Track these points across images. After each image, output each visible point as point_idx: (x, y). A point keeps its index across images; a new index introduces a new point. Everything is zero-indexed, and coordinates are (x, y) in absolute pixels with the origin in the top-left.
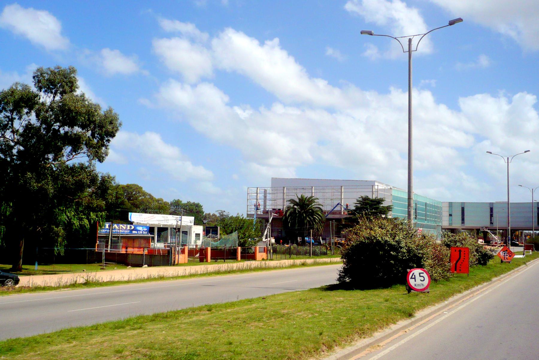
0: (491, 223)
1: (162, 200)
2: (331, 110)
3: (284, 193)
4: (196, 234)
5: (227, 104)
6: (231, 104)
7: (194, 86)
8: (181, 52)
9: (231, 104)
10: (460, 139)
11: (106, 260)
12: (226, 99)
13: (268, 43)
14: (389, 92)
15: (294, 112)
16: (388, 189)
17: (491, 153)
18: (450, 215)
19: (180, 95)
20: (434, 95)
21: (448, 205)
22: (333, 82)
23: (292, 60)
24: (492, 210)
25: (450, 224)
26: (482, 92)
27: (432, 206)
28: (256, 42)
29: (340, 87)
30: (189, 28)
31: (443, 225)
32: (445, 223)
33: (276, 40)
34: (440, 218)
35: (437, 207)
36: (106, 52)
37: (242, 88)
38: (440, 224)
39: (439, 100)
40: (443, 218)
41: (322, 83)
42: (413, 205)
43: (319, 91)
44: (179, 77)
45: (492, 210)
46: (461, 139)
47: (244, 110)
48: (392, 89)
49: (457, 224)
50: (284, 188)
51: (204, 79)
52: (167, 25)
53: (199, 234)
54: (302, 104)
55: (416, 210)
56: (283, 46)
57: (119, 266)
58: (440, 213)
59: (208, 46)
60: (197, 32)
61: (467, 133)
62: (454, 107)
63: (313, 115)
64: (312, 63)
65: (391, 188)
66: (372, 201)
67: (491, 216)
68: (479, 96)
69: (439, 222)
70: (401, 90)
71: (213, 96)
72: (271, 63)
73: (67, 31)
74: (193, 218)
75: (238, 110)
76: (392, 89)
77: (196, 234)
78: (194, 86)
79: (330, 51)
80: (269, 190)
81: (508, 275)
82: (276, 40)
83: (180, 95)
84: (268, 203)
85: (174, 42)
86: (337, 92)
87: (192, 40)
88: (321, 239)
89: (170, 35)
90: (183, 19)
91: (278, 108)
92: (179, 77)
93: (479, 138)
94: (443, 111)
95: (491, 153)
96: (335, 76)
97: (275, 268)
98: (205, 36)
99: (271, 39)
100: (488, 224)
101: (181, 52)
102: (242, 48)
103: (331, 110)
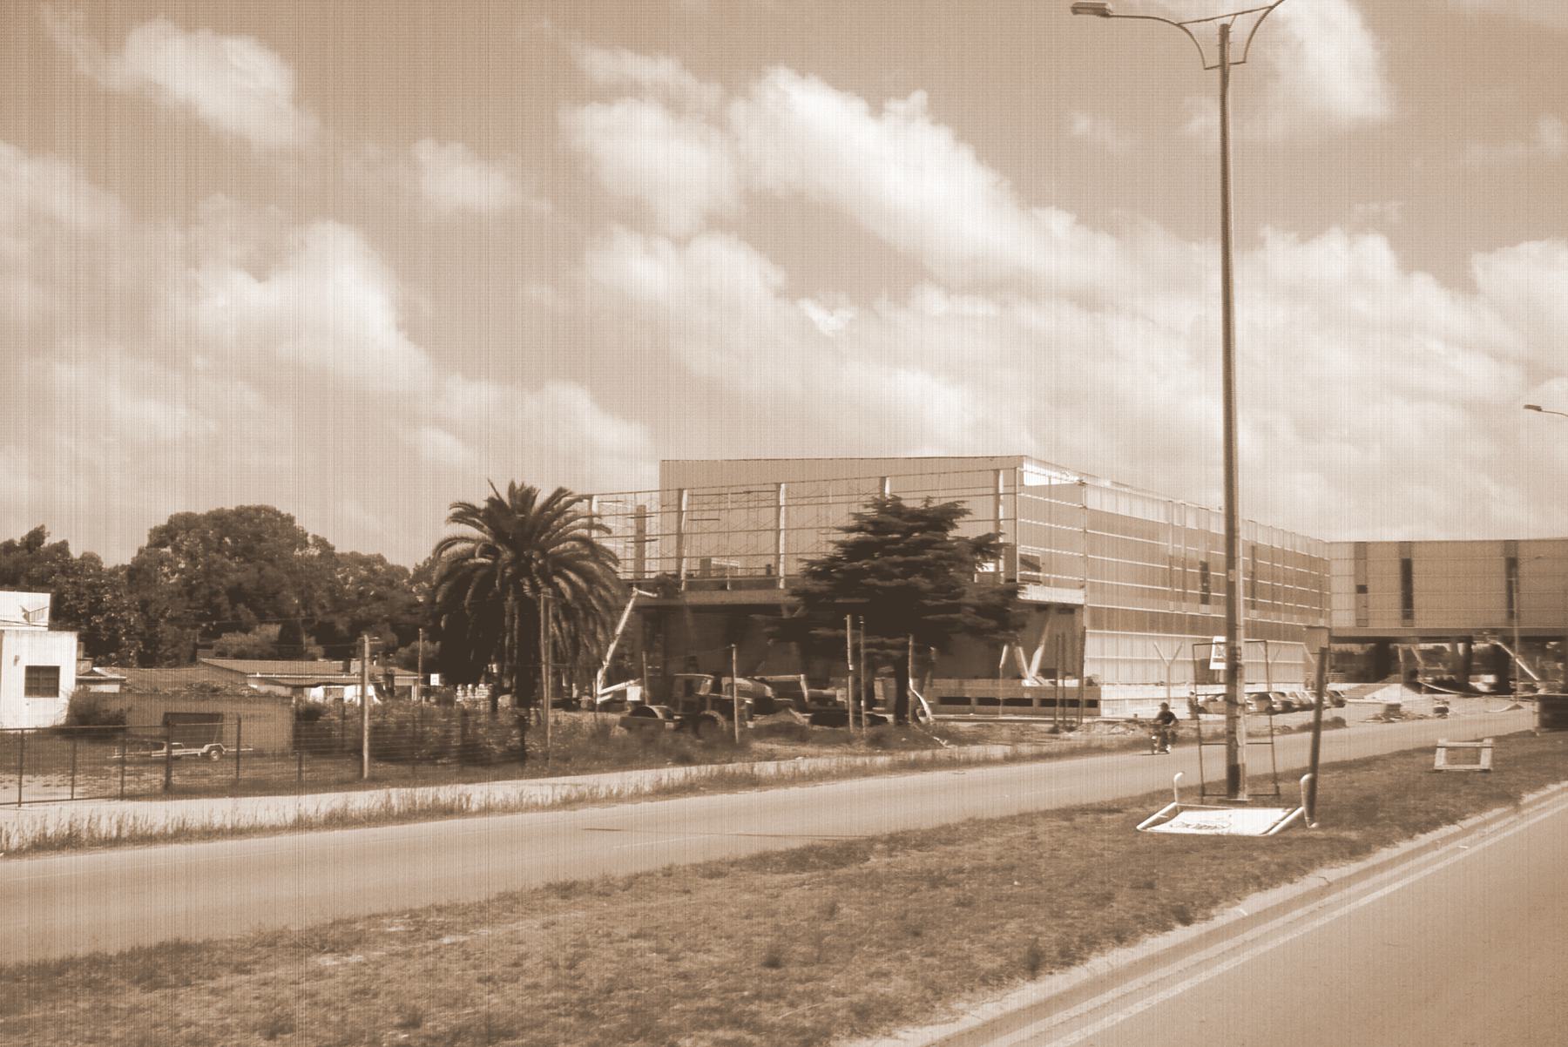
0: (1511, 614)
1: (380, 559)
2: (1088, 300)
3: (680, 512)
4: (31, 670)
5: (779, 294)
6: (792, 292)
7: (681, 243)
8: (644, 140)
9: (792, 292)
10: (1478, 374)
11: (379, 755)
12: (778, 277)
13: (896, 106)
14: (1262, 243)
15: (983, 309)
16: (1072, 486)
17: (1538, 409)
18: (1362, 589)
19: (642, 271)
20: (1395, 244)
21: (1348, 553)
22: (1091, 216)
23: (966, 154)
24: (1512, 564)
25: (1361, 621)
26: (1539, 237)
27: (1273, 553)
28: (859, 106)
29: (1114, 230)
30: (661, 70)
31: (1335, 624)
32: (1342, 616)
33: (919, 98)
34: (1321, 598)
35: (1311, 562)
36: (425, 150)
37: (821, 242)
38: (1322, 622)
39: (1412, 258)
40: (1334, 599)
41: (1059, 222)
42: (1242, 558)
43: (1051, 244)
44: (638, 217)
45: (1512, 564)
46: (1479, 375)
47: (831, 308)
48: (1267, 232)
49: (1385, 621)
50: (681, 491)
51: (715, 223)
52: (600, 63)
53: (54, 671)
54: (1000, 285)
55: (1253, 575)
56: (939, 113)
57: (472, 769)
58: (1322, 584)
59: (719, 121)
60: (688, 80)
61: (1498, 356)
62: (1459, 282)
63: (1031, 316)
64: (1028, 163)
65: (1082, 484)
66: (915, 515)
67: (1511, 589)
68: (1532, 248)
69: (1320, 614)
70: (1293, 236)
71: (741, 272)
72: (906, 165)
73: (313, 90)
74: (43, 600)
75: (815, 312)
76: (1267, 232)
77: (31, 670)
78: (681, 243)
79: (1082, 124)
80: (653, 505)
81: (1304, 899)
82: (919, 98)
83: (642, 271)
84: (651, 550)
85: (619, 112)
86: (1105, 244)
87: (674, 105)
88: (803, 684)
89: (610, 93)
90: (645, 45)
91: (934, 302)
92: (638, 217)
93: (1536, 372)
94: (1427, 297)
95: (1538, 409)
96: (1094, 194)
97: (615, 798)
98: (711, 93)
99: (904, 95)
100: (1498, 619)
101: (644, 140)
102: (823, 126)
103: (1088, 300)
